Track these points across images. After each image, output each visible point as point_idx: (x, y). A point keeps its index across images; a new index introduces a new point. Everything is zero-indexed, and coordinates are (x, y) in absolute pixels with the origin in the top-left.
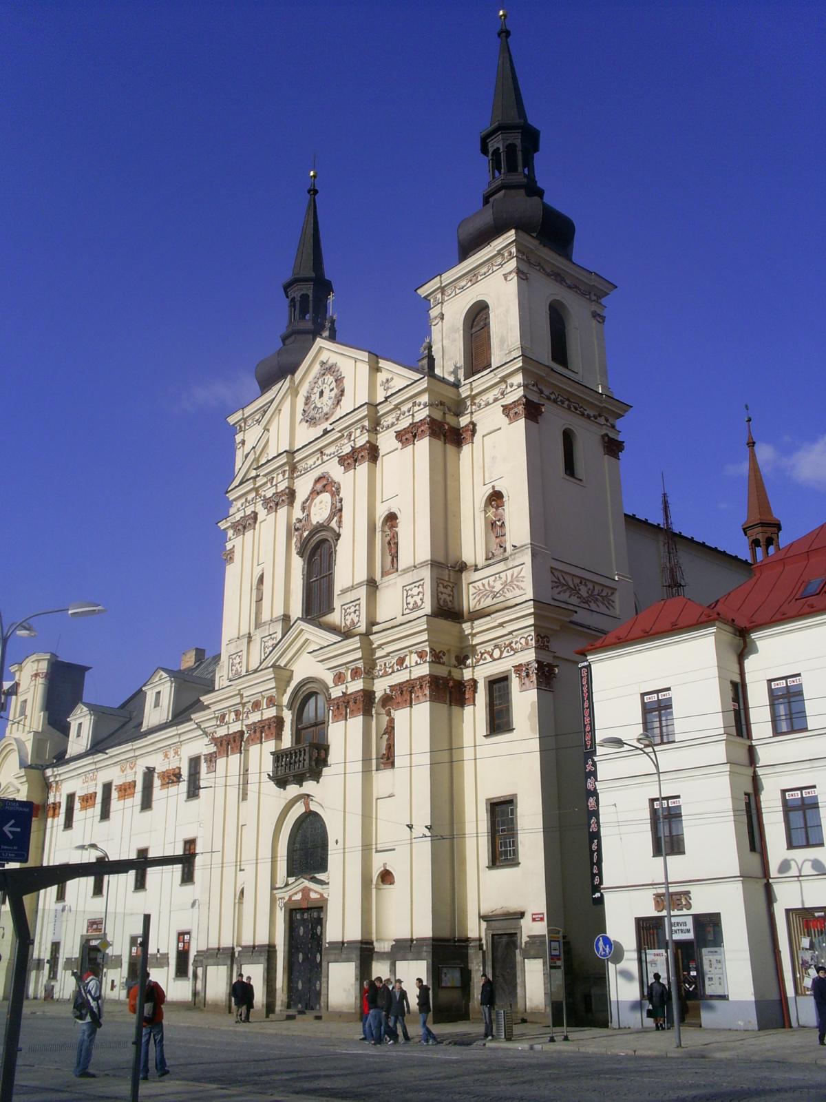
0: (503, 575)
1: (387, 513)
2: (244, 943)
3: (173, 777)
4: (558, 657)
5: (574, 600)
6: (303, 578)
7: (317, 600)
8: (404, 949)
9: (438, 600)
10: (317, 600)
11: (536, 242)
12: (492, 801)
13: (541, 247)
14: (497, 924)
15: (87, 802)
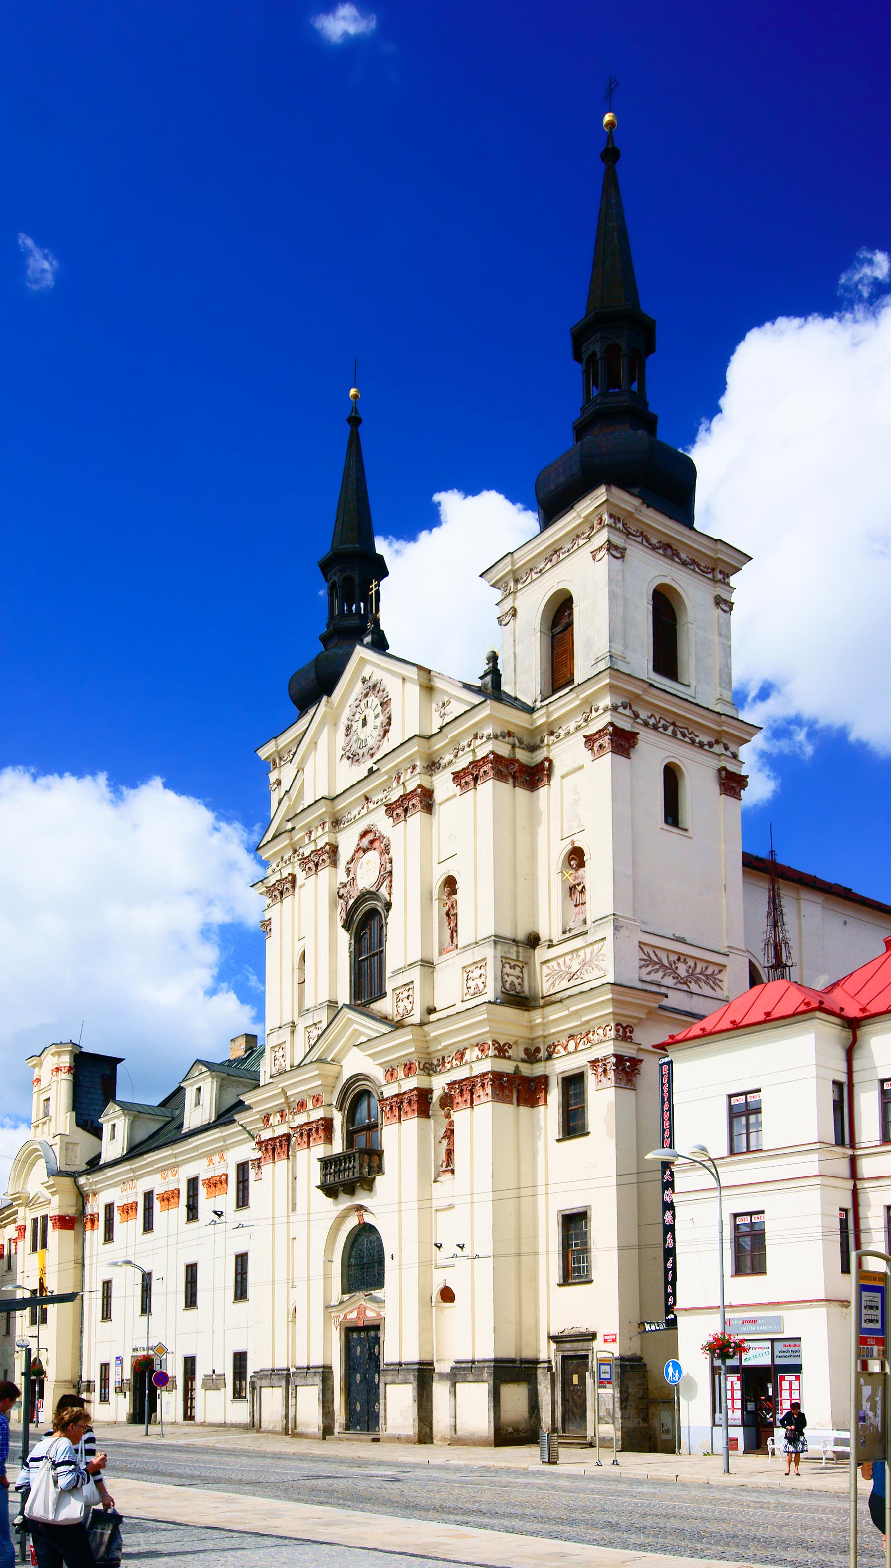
0: (581, 953)
1: (445, 876)
2: (298, 1364)
3: (216, 1184)
4: (643, 1050)
5: (669, 981)
6: (350, 956)
7: (367, 982)
8: (463, 1371)
9: (504, 982)
10: (367, 982)
11: (636, 502)
12: (565, 1213)
13: (644, 509)
14: (568, 1346)
15: (128, 1213)
